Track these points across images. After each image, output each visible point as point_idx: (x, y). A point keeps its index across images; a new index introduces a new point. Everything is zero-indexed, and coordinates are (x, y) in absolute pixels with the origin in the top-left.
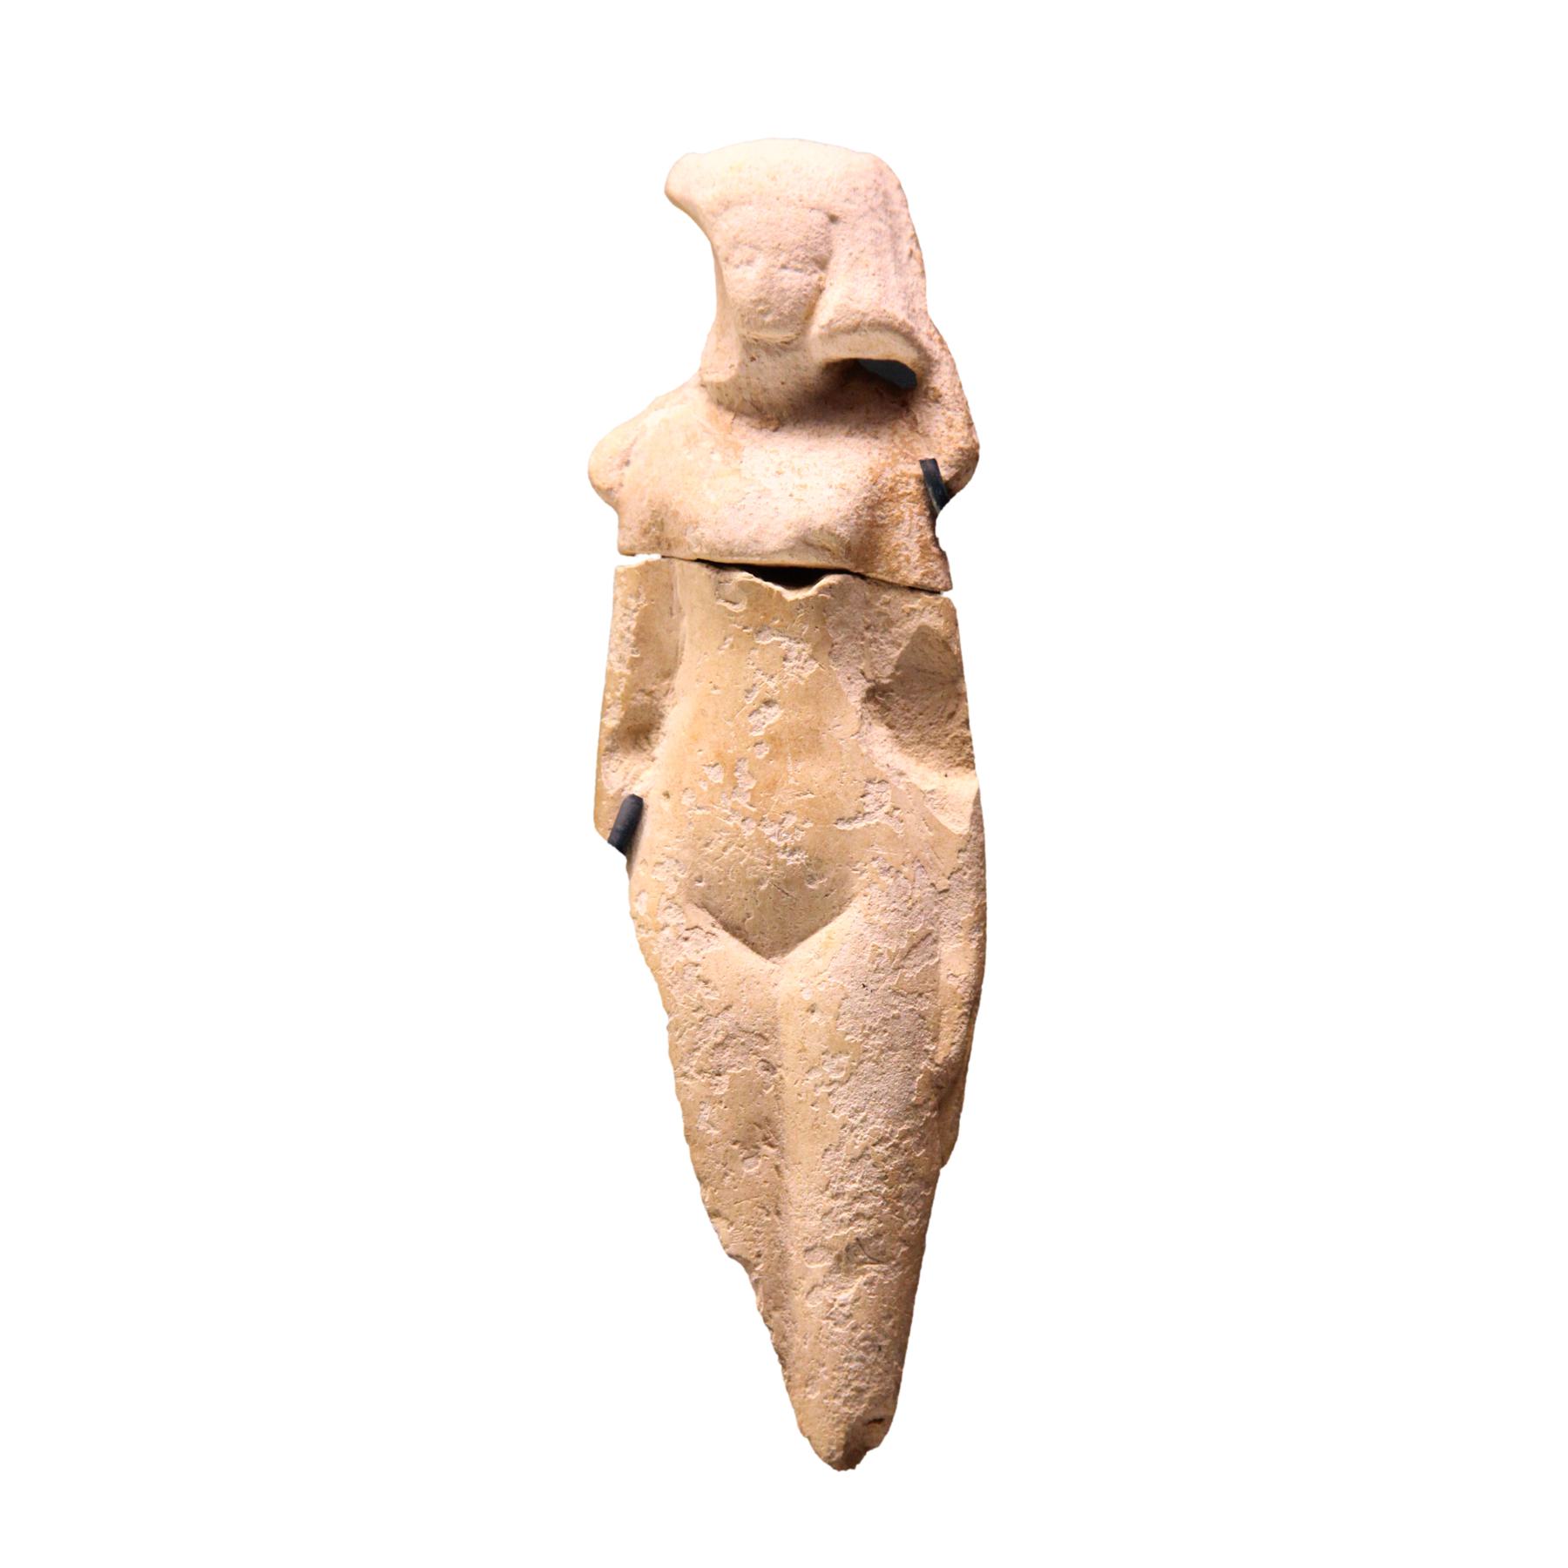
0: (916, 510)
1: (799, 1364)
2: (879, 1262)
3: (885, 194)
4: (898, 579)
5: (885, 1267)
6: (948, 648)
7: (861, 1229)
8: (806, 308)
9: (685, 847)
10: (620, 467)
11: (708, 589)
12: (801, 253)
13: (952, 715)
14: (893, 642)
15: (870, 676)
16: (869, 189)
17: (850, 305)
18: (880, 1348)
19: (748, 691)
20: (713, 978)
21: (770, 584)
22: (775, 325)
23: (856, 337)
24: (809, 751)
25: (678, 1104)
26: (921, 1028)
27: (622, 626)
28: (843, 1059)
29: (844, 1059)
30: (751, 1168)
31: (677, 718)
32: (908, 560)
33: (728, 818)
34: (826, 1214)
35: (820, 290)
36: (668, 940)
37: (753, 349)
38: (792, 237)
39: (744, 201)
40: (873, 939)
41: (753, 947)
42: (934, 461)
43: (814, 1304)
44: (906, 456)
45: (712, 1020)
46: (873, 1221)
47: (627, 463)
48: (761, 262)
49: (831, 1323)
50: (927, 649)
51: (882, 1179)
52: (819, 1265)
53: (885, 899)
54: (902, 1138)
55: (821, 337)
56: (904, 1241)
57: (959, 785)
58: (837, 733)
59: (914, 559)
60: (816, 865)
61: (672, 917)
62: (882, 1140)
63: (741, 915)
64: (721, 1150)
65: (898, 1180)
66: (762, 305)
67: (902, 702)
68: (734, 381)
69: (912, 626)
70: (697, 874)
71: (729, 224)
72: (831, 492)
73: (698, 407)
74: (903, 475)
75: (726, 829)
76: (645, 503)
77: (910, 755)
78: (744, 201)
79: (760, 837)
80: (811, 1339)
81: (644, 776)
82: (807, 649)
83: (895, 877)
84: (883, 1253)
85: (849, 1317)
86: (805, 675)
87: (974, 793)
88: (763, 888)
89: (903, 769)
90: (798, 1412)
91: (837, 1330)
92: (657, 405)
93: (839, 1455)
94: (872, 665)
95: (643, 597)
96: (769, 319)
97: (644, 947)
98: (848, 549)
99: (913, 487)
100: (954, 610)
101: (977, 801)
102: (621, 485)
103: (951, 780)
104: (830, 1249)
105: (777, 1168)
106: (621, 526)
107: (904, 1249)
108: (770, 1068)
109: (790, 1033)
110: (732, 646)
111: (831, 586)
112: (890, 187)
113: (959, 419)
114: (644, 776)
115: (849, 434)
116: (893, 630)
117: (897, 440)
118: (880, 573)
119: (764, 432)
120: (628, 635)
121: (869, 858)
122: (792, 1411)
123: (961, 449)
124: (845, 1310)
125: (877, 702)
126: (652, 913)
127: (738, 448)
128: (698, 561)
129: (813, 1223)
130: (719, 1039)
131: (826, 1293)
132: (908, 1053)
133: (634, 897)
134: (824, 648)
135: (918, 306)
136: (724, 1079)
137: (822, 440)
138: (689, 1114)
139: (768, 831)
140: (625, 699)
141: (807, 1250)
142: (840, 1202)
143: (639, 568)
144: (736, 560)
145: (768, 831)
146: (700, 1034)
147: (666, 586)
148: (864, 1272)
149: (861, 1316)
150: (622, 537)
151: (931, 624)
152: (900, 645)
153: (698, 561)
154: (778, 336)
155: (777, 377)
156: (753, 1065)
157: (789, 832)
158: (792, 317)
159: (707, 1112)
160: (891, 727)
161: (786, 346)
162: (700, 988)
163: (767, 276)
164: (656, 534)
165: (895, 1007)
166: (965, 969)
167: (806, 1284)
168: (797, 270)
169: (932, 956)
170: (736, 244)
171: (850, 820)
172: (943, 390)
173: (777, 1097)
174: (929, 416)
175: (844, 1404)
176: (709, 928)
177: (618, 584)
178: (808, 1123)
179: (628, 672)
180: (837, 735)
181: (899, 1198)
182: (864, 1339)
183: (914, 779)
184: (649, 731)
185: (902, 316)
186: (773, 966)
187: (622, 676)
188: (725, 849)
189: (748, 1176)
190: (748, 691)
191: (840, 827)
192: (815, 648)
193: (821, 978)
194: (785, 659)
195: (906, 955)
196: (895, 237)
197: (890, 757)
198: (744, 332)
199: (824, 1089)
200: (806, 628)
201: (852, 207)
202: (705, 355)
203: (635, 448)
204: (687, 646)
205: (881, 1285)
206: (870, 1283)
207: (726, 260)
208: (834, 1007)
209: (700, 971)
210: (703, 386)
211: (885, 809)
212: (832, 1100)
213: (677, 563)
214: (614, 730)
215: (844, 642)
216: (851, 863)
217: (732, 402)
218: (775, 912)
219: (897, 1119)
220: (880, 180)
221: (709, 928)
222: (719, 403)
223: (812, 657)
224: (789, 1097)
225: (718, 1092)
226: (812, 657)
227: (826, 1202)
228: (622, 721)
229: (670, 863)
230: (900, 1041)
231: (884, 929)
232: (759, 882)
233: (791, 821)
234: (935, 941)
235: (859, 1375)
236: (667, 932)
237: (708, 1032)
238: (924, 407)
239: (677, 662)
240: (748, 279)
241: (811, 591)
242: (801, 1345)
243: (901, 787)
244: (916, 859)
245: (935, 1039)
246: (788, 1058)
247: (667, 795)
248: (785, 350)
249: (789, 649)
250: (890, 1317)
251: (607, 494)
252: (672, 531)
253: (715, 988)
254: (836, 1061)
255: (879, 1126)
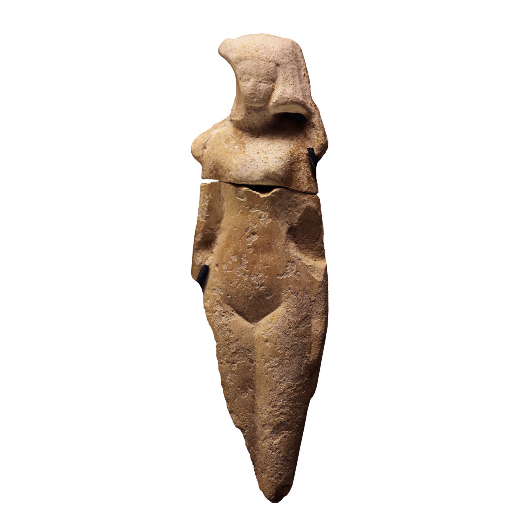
0: (306, 166)
1: (260, 465)
2: (288, 430)
3: (296, 55)
4: (300, 189)
5: (290, 432)
6: (317, 213)
7: (282, 418)
8: (269, 95)
9: (223, 284)
10: (202, 149)
11: (233, 193)
12: (266, 77)
13: (318, 239)
14: (298, 211)
15: (289, 223)
16: (290, 53)
17: (283, 91)
18: (288, 460)
19: (247, 229)
20: (233, 329)
21: (255, 192)
22: (257, 102)
23: (285, 106)
24: (267, 251)
25: (219, 374)
26: (304, 348)
27: (203, 205)
28: (277, 359)
29: (277, 359)
30: (244, 397)
31: (221, 238)
32: (303, 183)
33: (238, 274)
34: (270, 413)
35: (273, 90)
36: (217, 316)
37: (249, 110)
38: (263, 72)
39: (247, 59)
40: (289, 317)
41: (247, 319)
42: (312, 149)
43: (265, 444)
44: (303, 147)
45: (232, 344)
46: (287, 415)
47: (205, 148)
48: (252, 80)
49: (271, 451)
50: (310, 214)
51: (290, 401)
52: (267, 431)
53: (293, 303)
54: (297, 387)
55: (273, 106)
56: (297, 423)
57: (319, 264)
58: (278, 244)
59: (305, 183)
60: (269, 290)
61: (218, 308)
62: (290, 387)
63: (243, 308)
64: (234, 389)
65: (296, 401)
66: (253, 95)
67: (300, 234)
68: (242, 120)
69: (304, 206)
70: (227, 293)
71: (242, 66)
72: (276, 160)
73: (229, 129)
74: (302, 153)
75: (238, 278)
76: (211, 162)
77: (303, 253)
78: (247, 59)
79: (250, 280)
80: (264, 456)
81: (210, 259)
82: (267, 214)
83: (297, 296)
84: (290, 427)
85: (277, 449)
86: (267, 223)
87: (325, 266)
88: (250, 298)
89: (300, 257)
90: (259, 482)
91: (273, 453)
92: (215, 127)
93: (273, 497)
94: (290, 219)
95: (210, 195)
96: (255, 100)
97: (209, 318)
98: (282, 179)
99: (305, 157)
100: (319, 200)
101: (326, 270)
102: (203, 156)
103: (317, 262)
104: (271, 425)
105: (253, 396)
106: (203, 170)
107: (297, 426)
108: (252, 361)
109: (259, 349)
110: (241, 213)
111: (276, 193)
112: (298, 51)
113: (321, 133)
114: (210, 259)
115: (283, 139)
116: (298, 207)
117: (299, 141)
118: (293, 187)
119: (253, 138)
120: (205, 208)
121: (288, 289)
122: (257, 482)
123: (322, 144)
124: (276, 446)
125: (291, 234)
126: (211, 307)
127: (244, 144)
128: (230, 183)
129: (266, 416)
130: (234, 351)
131: (270, 440)
132: (300, 357)
133: (205, 301)
134: (274, 214)
135: (307, 94)
136: (236, 365)
137: (273, 141)
138: (223, 377)
139: (253, 279)
140: (203, 231)
141: (263, 425)
142: (275, 409)
143: (209, 185)
144: (243, 183)
145: (253, 279)
146: (227, 349)
147: (218, 191)
148: (283, 433)
149: (282, 448)
150: (203, 174)
151: (311, 205)
152: (300, 212)
153: (230, 183)
154: (258, 106)
155: (257, 119)
156: (246, 360)
157: (260, 279)
158: (263, 99)
159: (229, 376)
160: (296, 243)
161: (261, 109)
162: (228, 333)
163: (255, 85)
164: (214, 171)
165: (296, 341)
166: (320, 328)
167: (262, 437)
168: (265, 83)
169: (309, 323)
170: (244, 73)
171: (281, 275)
172: (316, 123)
173: (254, 372)
174: (311, 132)
175: (275, 479)
176: (231, 312)
177: (201, 190)
178: (264, 381)
179: (204, 221)
180: (278, 245)
181: (296, 408)
182: (282, 457)
183: (304, 262)
184: (211, 243)
185: (301, 99)
186: (253, 326)
187: (202, 222)
188: (237, 284)
189: (243, 399)
190: (247, 229)
191: (278, 278)
192: (270, 214)
193: (270, 330)
194: (260, 218)
195: (300, 323)
196: (299, 70)
197: (296, 253)
198: (246, 104)
199: (270, 369)
200: (268, 207)
201: (285, 61)
202: (232, 110)
203: (208, 142)
204: (225, 212)
205: (289, 438)
206: (285, 437)
207: (240, 79)
208: (274, 341)
209: (228, 327)
210: (231, 120)
211: (294, 272)
212: (273, 373)
213: (222, 183)
214: (199, 242)
215: (280, 212)
216: (281, 290)
217: (242, 127)
218: (255, 307)
219: (294, 380)
220: (294, 50)
221: (231, 312)
222: (237, 127)
223: (269, 217)
224: (258, 372)
225: (233, 369)
226: (269, 217)
227: (270, 409)
228: (202, 239)
229: (218, 289)
230: (297, 353)
231: (293, 313)
232: (249, 296)
233: (261, 275)
234: (310, 318)
235: (281, 469)
236: (216, 313)
237: (230, 348)
238: (309, 129)
239: (222, 218)
240: (248, 85)
241: (269, 194)
242: (261, 458)
243: (299, 264)
244: (304, 289)
245: (310, 353)
246: (258, 357)
247: (217, 265)
248: (261, 110)
249: (261, 214)
250: (292, 449)
251: (198, 158)
252: (221, 172)
253: (233, 333)
254: (275, 359)
255: (289, 382)
